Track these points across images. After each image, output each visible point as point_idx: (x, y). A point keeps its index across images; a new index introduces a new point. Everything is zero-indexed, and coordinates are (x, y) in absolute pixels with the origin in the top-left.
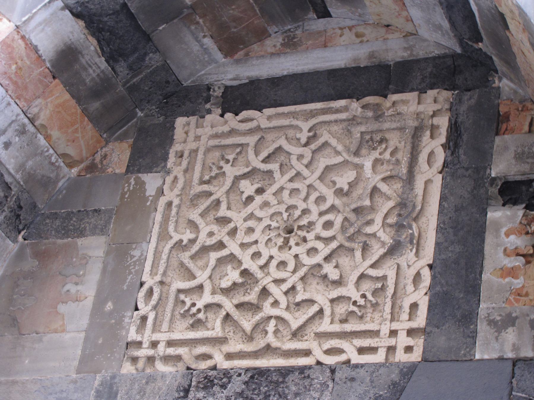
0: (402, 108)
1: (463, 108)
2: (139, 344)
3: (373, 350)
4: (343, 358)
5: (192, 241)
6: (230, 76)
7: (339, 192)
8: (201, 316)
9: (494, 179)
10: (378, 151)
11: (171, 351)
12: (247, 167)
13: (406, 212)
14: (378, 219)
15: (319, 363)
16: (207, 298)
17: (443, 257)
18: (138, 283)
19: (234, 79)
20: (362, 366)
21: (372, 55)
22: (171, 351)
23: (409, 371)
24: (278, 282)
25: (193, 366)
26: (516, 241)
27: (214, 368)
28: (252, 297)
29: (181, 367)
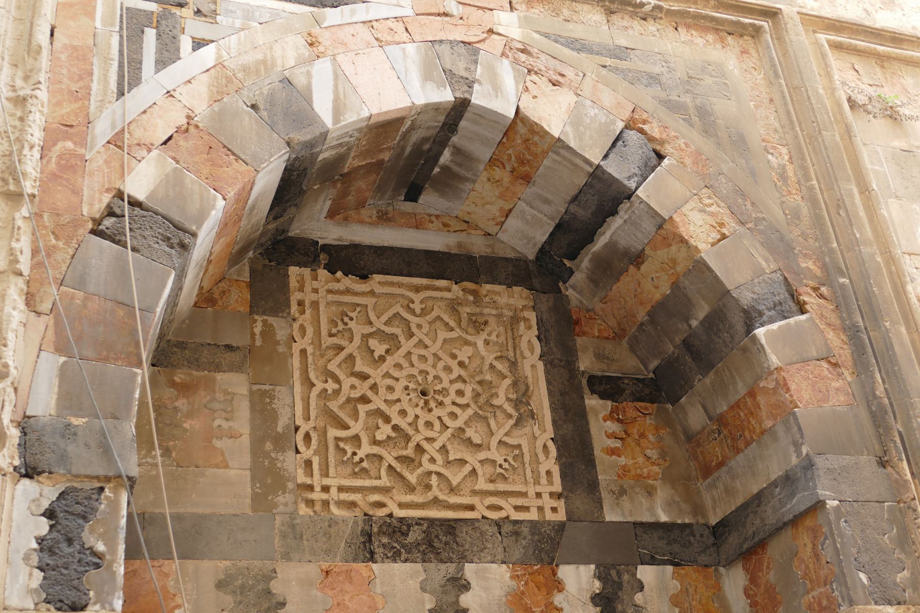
0: (497, 298)
1: (544, 308)
2: (311, 488)
3: (526, 509)
4: (503, 514)
5: (337, 392)
6: (335, 237)
7: (461, 364)
8: (365, 464)
9: (583, 372)
10: (486, 332)
11: (344, 496)
12: (267, 320)
13: (522, 398)
14: (502, 394)
15: (483, 517)
16: (366, 449)
17: (561, 432)
18: (293, 429)
19: (338, 240)
20: (522, 522)
21: (460, 245)
22: (344, 496)
23: (560, 527)
24: (430, 440)
25: (371, 513)
26: (612, 426)
27: (390, 515)
28: (410, 452)
29: (358, 512)
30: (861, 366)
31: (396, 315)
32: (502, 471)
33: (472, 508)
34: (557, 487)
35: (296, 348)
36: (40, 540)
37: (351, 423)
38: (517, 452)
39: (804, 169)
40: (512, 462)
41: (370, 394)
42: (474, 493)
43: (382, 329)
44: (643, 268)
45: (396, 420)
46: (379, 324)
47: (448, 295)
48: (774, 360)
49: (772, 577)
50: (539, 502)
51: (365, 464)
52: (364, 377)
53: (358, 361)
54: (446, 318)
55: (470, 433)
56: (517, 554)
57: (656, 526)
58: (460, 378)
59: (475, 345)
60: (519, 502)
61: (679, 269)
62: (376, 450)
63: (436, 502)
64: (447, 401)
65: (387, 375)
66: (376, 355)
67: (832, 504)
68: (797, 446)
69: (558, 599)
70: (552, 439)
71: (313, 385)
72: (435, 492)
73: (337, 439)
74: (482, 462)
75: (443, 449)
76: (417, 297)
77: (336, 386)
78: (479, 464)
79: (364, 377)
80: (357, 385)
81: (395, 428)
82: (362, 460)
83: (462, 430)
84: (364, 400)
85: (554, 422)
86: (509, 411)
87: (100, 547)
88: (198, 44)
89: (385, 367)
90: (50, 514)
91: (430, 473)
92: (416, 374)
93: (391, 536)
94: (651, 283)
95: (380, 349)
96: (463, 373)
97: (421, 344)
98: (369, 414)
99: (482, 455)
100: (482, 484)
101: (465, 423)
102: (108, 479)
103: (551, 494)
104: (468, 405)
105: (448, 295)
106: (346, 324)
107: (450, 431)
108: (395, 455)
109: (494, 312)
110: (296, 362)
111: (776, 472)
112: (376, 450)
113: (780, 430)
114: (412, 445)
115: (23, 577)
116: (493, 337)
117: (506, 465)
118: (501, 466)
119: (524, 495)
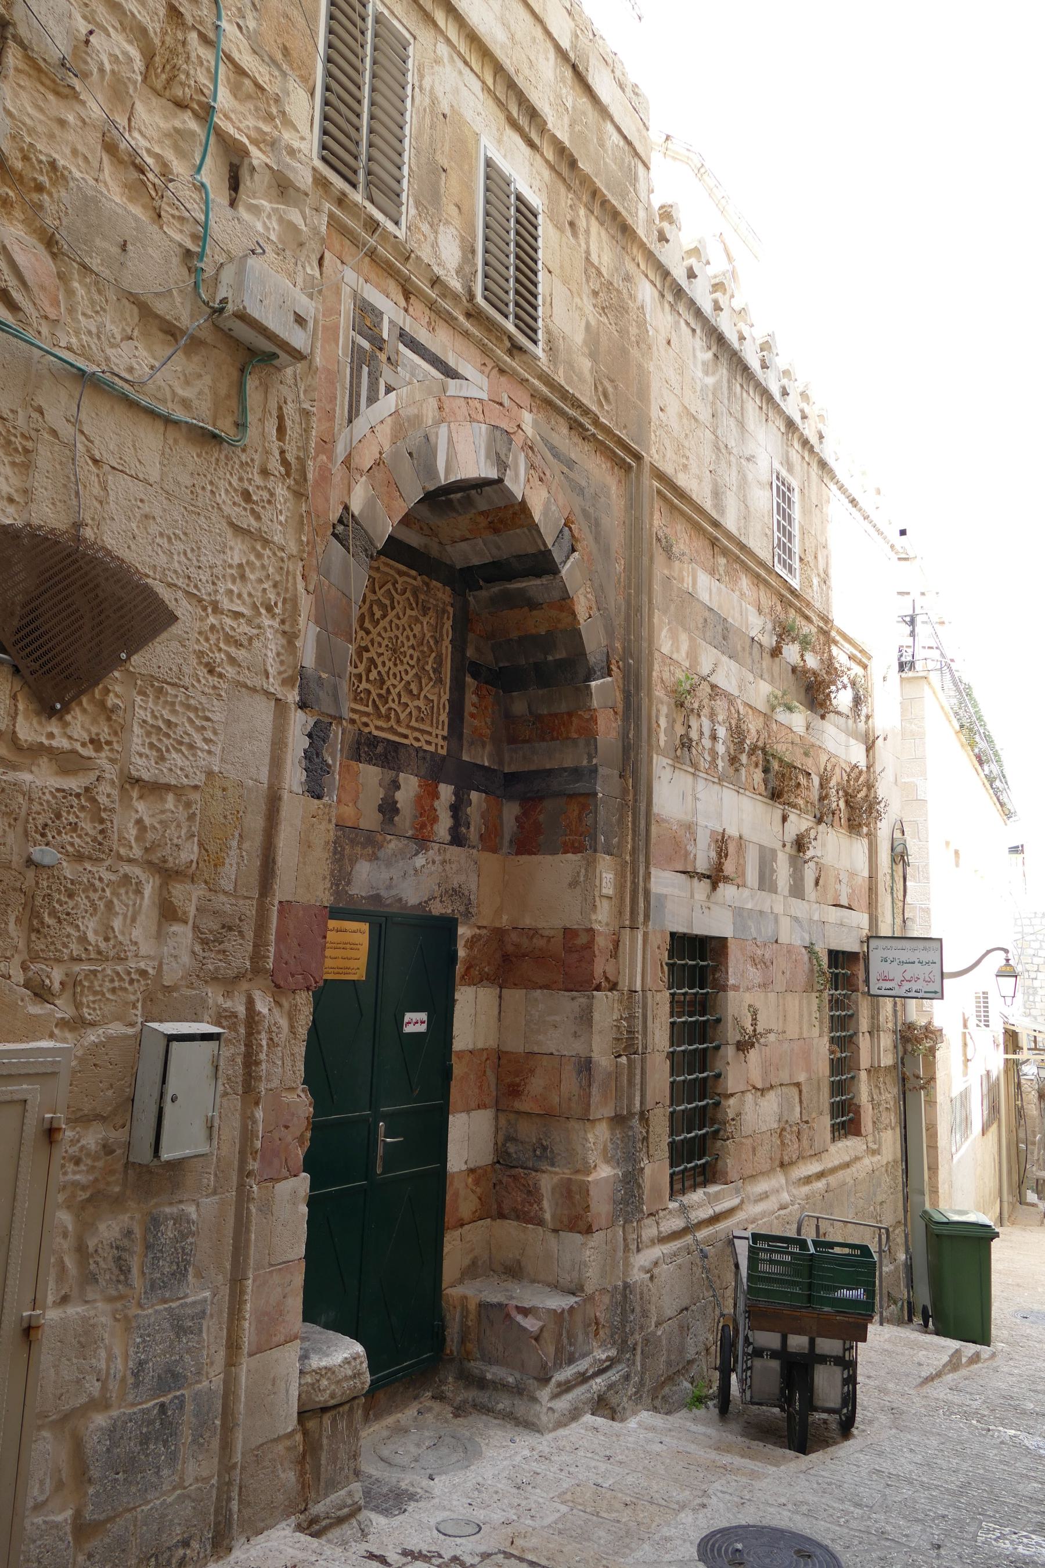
30: (626, 718)
33: (406, 737)
34: (445, 733)
36: (305, 751)
39: (629, 579)
44: (535, 612)
47: (414, 583)
48: (595, 704)
49: (541, 818)
56: (423, 772)
57: (483, 767)
60: (428, 738)
61: (559, 626)
63: (391, 730)
67: (600, 795)
68: (590, 758)
69: (436, 803)
75: (399, 695)
87: (330, 762)
88: (389, 389)
90: (310, 735)
93: (368, 746)
94: (537, 623)
102: (335, 718)
105: (414, 583)
111: (568, 763)
113: (582, 743)
115: (298, 774)
119: (430, 734)
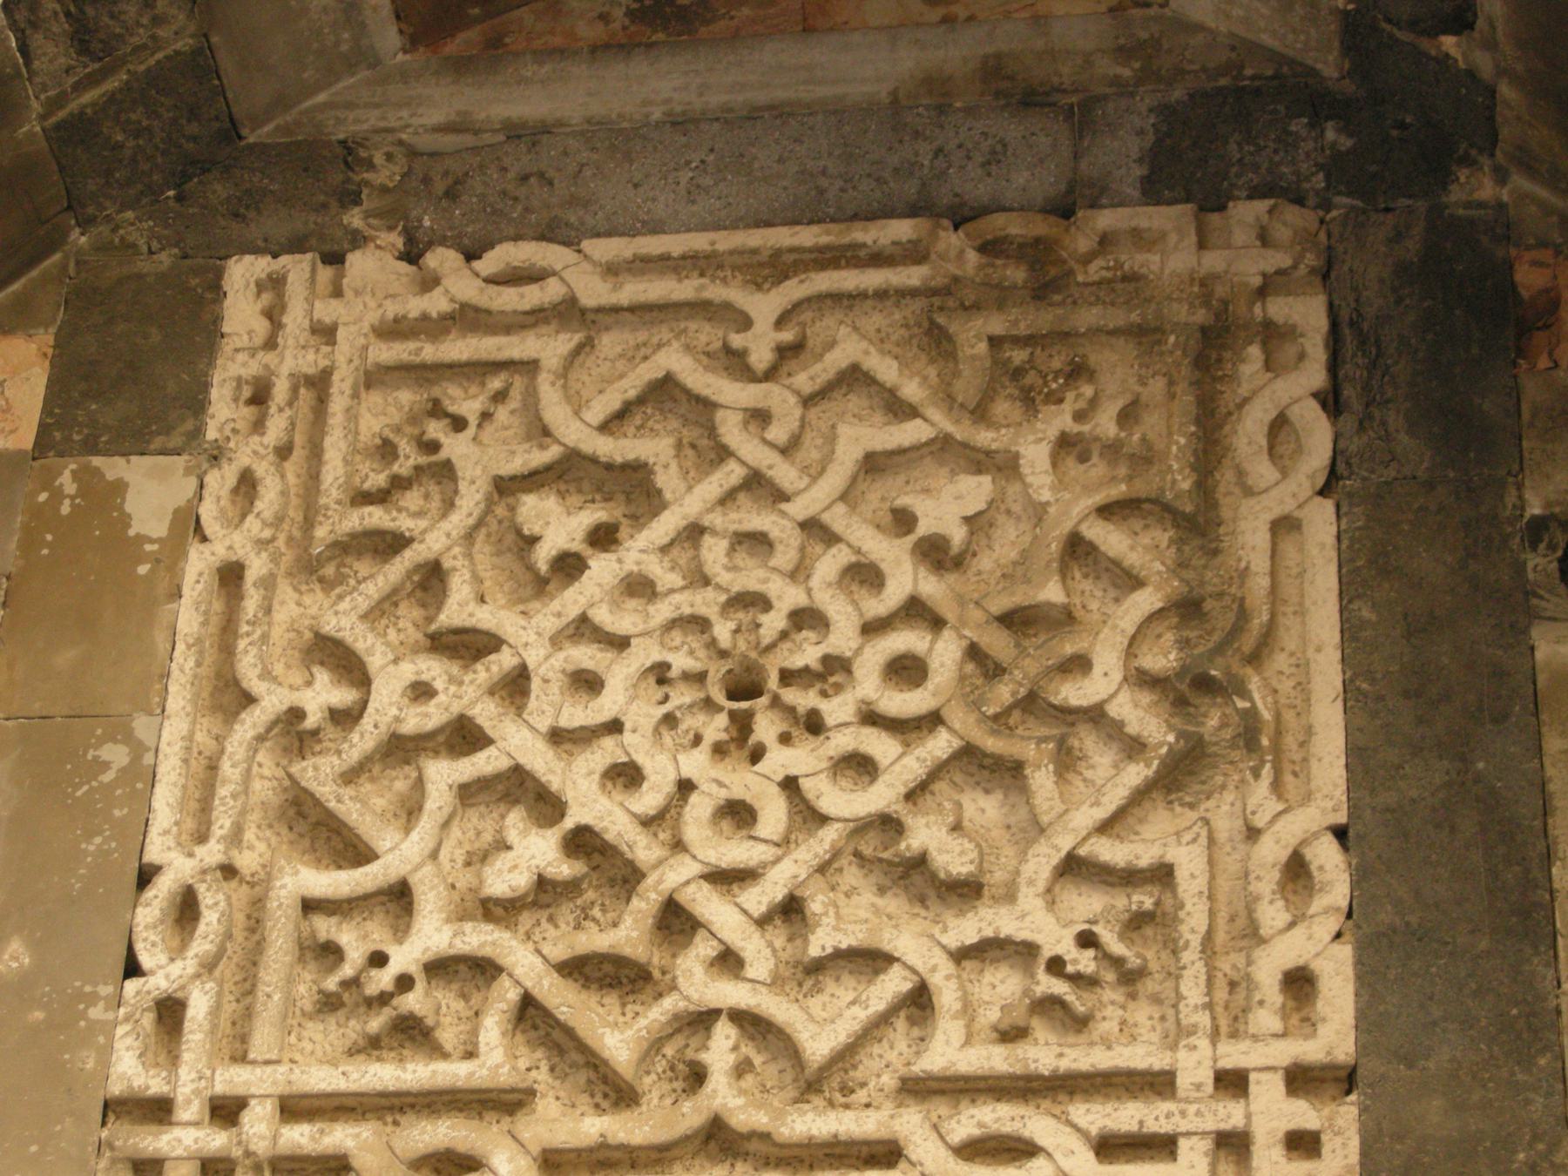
5: (345, 718)
7: (935, 553)
8: (412, 1001)
10: (1068, 407)
16: (432, 933)
24: (727, 879)
28: (627, 932)
31: (665, 390)
32: (1059, 987)
34: (1334, 1035)
35: (199, 564)
37: (383, 838)
38: (1144, 899)
40: (1117, 947)
41: (486, 713)
42: (917, 1089)
43: (587, 448)
45: (589, 803)
46: (576, 431)
47: (912, 276)
50: (1230, 1114)
51: (412, 1001)
52: (468, 646)
53: (460, 589)
54: (886, 369)
55: (924, 833)
58: (916, 611)
59: (1004, 466)
60: (1127, 1116)
62: (478, 938)
64: (837, 709)
65: (583, 628)
66: (543, 556)
70: (1340, 833)
71: (249, 699)
72: (724, 1096)
73: (310, 906)
74: (961, 955)
76: (764, 306)
77: (343, 696)
78: (946, 966)
79: (468, 646)
80: (439, 685)
81: (582, 842)
82: (404, 983)
83: (889, 824)
84: (465, 736)
85: (1357, 755)
86: (1132, 729)
89: (572, 600)
91: (701, 1020)
92: (712, 612)
95: (558, 524)
96: (931, 587)
97: (756, 484)
98: (468, 793)
99: (967, 928)
100: (948, 1051)
101: (910, 796)
103: (1300, 1079)
104: (934, 720)
106: (433, 447)
107: (830, 835)
108: (559, 952)
109: (1117, 318)
110: (189, 617)
112: (478, 938)
114: (645, 903)
116: (1106, 424)
117: (1085, 961)
118: (1056, 966)
119: (1159, 1084)
